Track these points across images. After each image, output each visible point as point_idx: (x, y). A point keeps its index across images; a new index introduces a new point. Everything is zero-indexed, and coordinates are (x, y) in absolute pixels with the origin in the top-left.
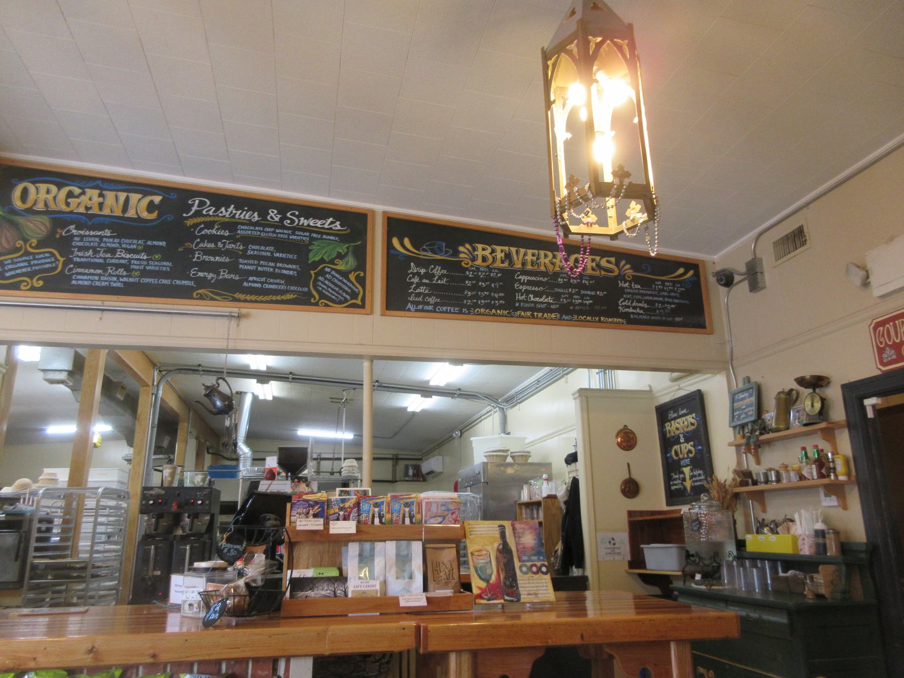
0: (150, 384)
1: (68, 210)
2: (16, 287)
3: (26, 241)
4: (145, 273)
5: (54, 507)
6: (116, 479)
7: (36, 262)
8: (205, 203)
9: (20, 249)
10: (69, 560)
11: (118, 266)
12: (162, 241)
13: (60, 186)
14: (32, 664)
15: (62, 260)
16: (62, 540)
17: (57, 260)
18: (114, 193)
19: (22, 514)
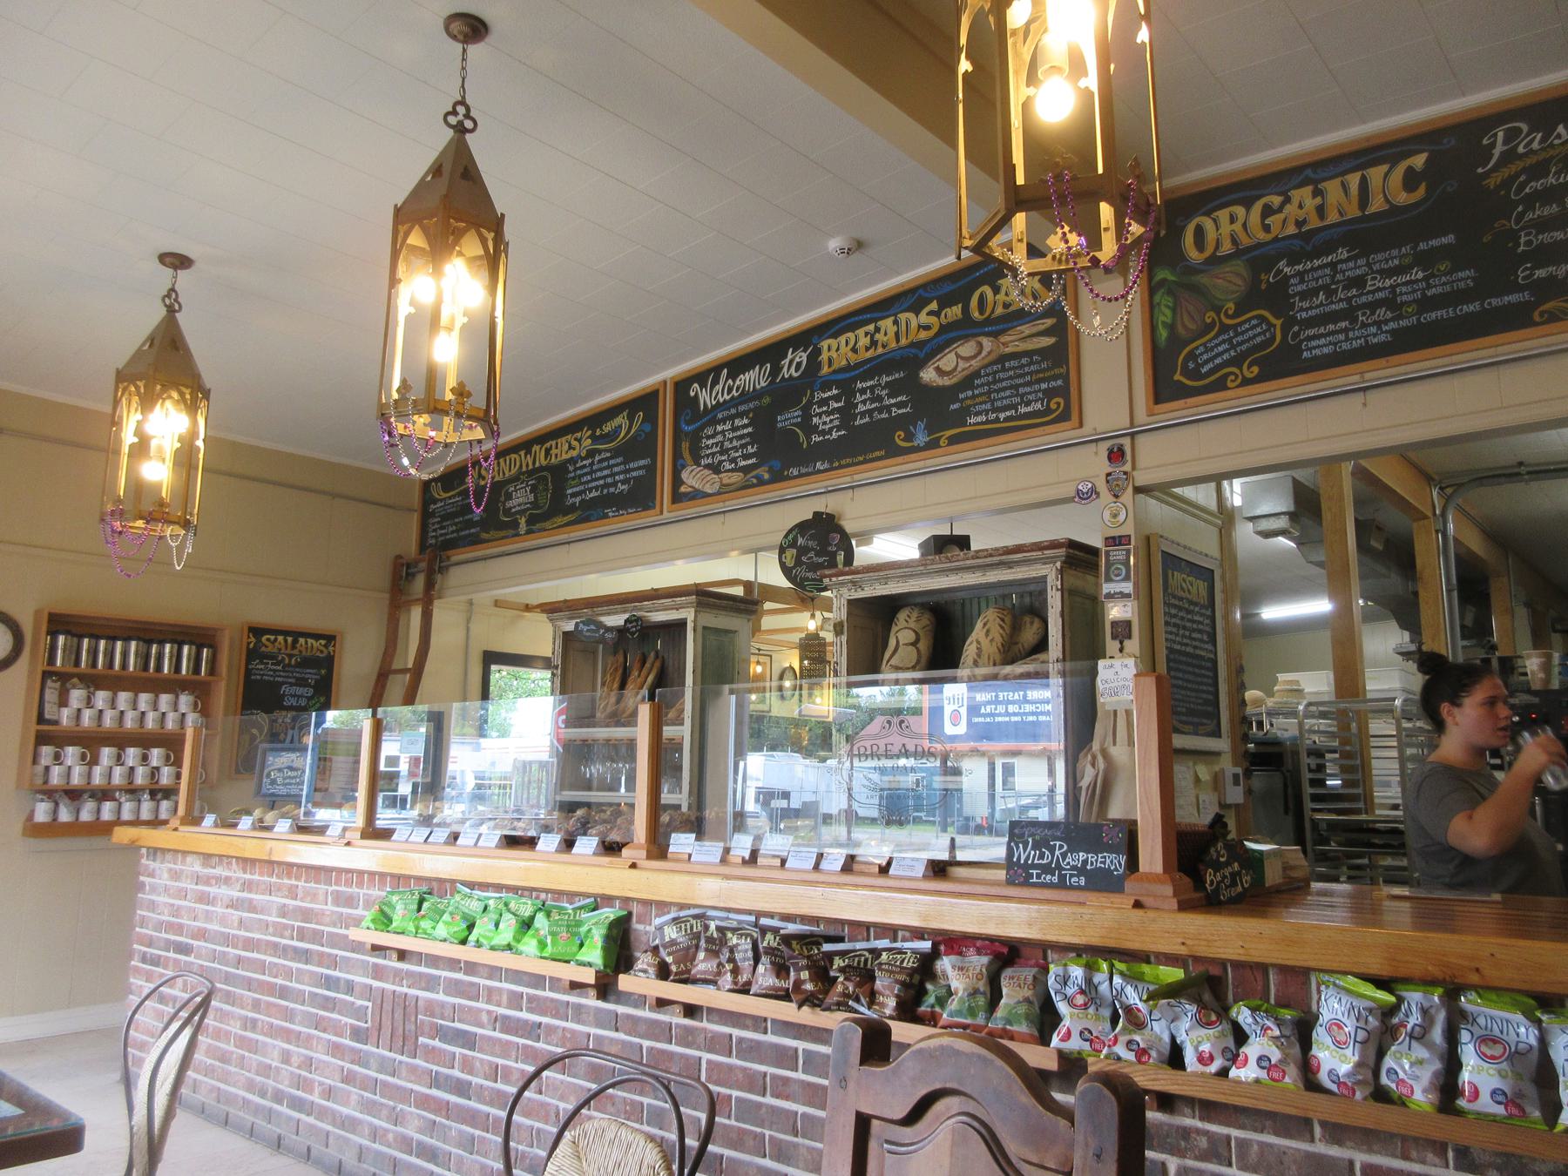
0: (1429, 514)
1: (1269, 237)
2: (1220, 385)
3: (1217, 310)
4: (1426, 304)
5: (1319, 730)
6: (1397, 685)
7: (1240, 339)
8: (1520, 130)
9: (1211, 326)
10: (1363, 817)
11: (1373, 306)
12: (1445, 235)
13: (1248, 204)
14: (1474, 978)
15: (1278, 323)
16: (1346, 784)
17: (1270, 325)
18: (1337, 181)
19: (1277, 743)
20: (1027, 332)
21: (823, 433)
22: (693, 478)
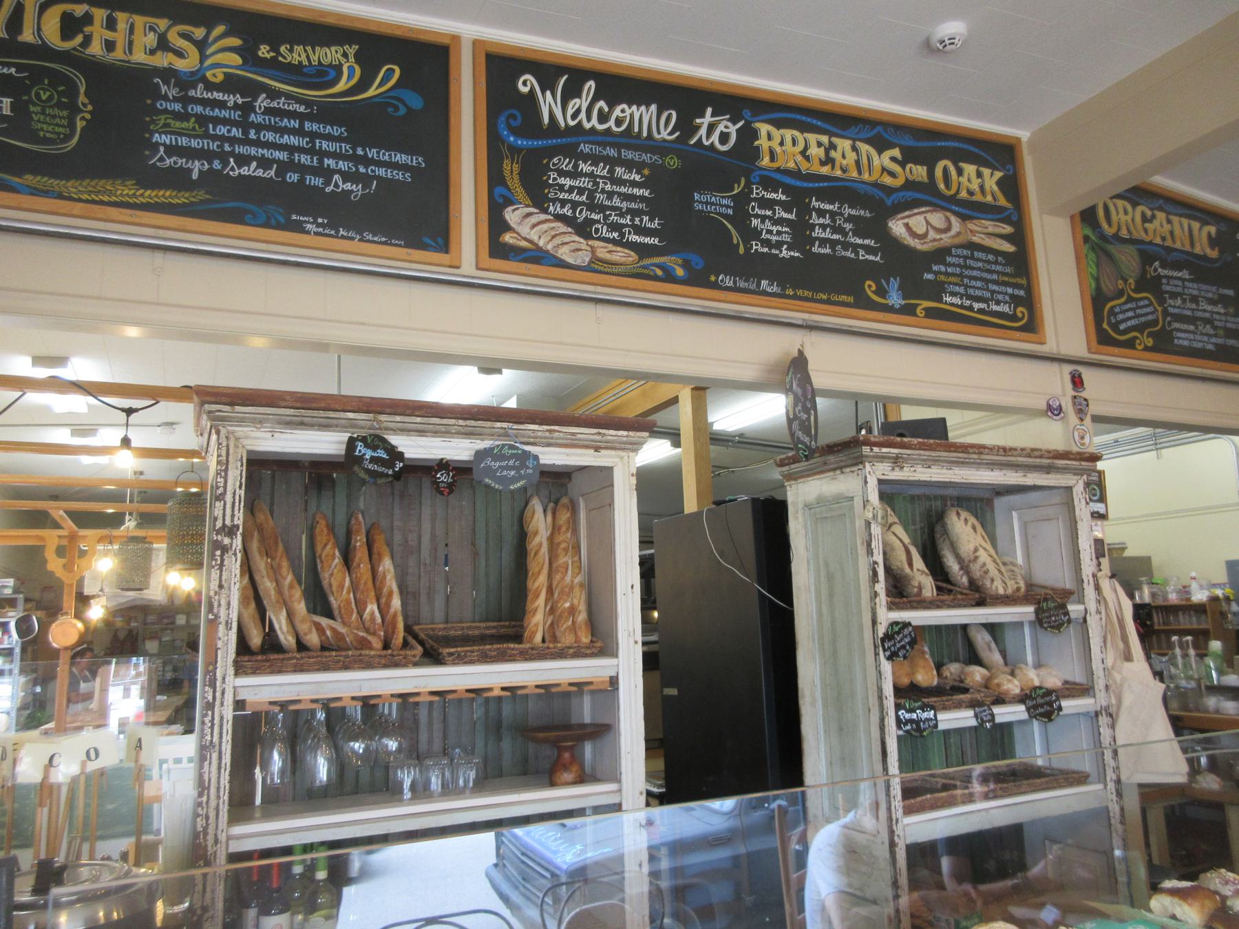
2: (1130, 344)
15: (1160, 309)
20: (990, 230)
21: (767, 243)
22: (525, 224)
